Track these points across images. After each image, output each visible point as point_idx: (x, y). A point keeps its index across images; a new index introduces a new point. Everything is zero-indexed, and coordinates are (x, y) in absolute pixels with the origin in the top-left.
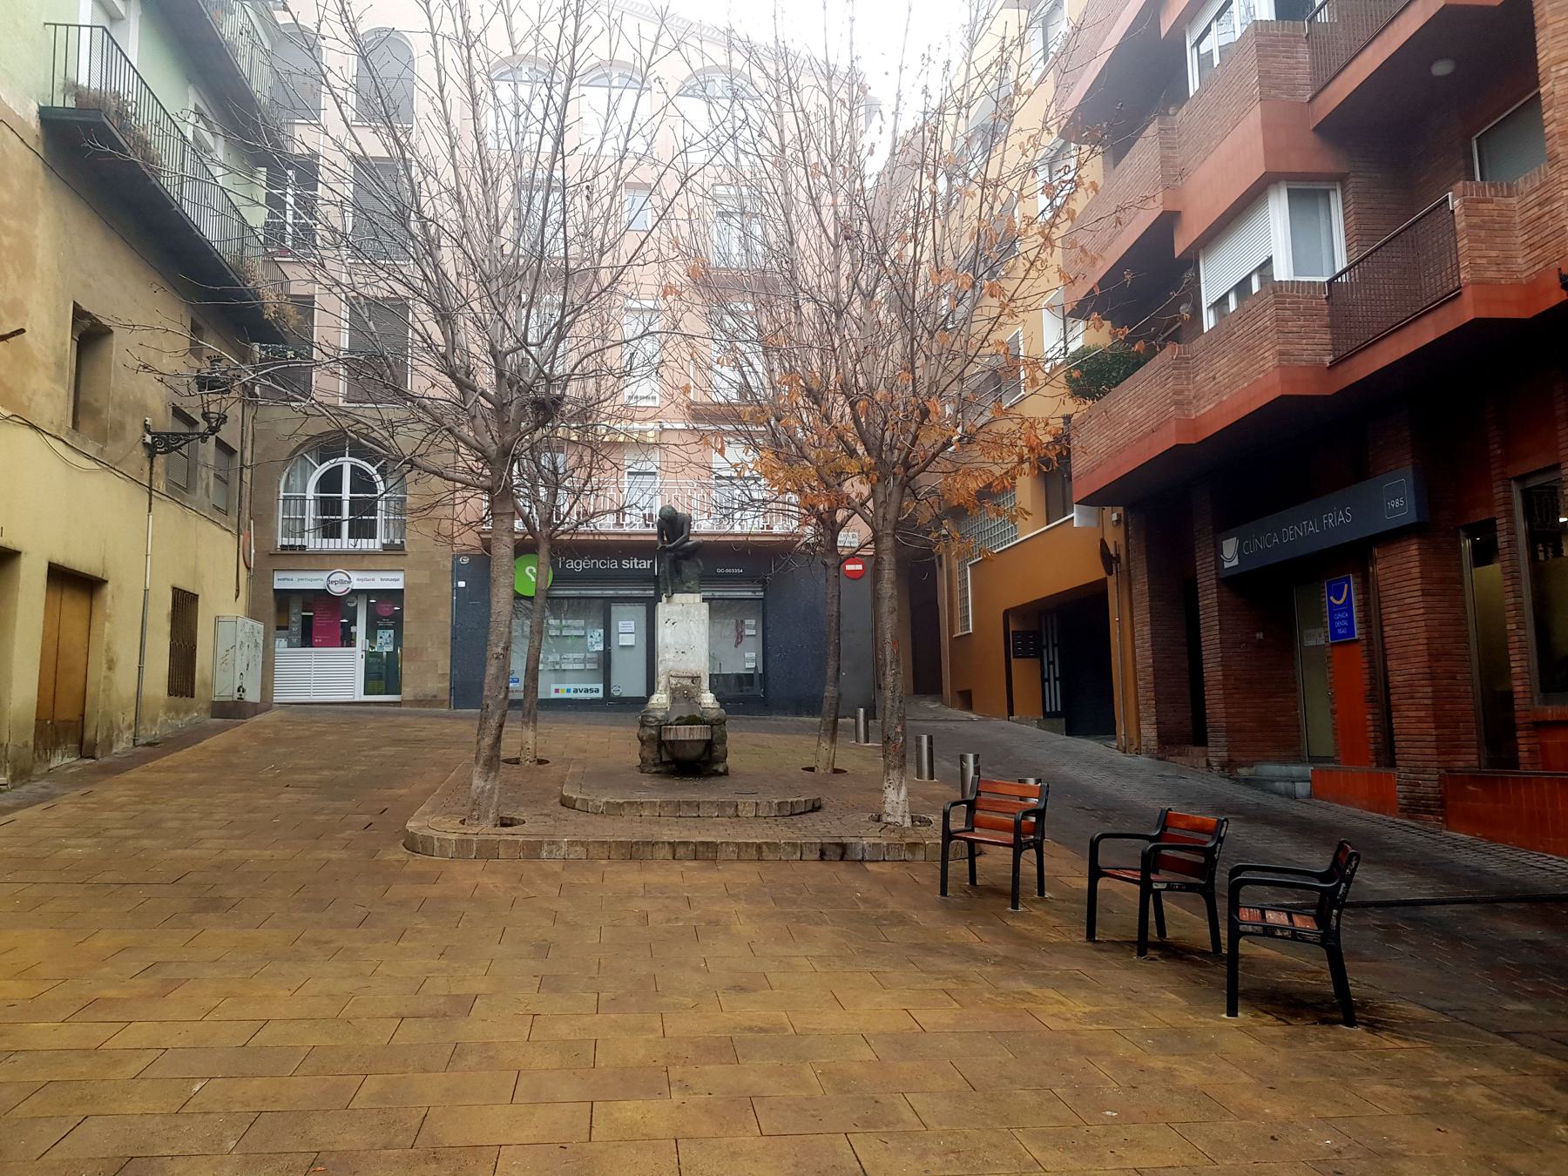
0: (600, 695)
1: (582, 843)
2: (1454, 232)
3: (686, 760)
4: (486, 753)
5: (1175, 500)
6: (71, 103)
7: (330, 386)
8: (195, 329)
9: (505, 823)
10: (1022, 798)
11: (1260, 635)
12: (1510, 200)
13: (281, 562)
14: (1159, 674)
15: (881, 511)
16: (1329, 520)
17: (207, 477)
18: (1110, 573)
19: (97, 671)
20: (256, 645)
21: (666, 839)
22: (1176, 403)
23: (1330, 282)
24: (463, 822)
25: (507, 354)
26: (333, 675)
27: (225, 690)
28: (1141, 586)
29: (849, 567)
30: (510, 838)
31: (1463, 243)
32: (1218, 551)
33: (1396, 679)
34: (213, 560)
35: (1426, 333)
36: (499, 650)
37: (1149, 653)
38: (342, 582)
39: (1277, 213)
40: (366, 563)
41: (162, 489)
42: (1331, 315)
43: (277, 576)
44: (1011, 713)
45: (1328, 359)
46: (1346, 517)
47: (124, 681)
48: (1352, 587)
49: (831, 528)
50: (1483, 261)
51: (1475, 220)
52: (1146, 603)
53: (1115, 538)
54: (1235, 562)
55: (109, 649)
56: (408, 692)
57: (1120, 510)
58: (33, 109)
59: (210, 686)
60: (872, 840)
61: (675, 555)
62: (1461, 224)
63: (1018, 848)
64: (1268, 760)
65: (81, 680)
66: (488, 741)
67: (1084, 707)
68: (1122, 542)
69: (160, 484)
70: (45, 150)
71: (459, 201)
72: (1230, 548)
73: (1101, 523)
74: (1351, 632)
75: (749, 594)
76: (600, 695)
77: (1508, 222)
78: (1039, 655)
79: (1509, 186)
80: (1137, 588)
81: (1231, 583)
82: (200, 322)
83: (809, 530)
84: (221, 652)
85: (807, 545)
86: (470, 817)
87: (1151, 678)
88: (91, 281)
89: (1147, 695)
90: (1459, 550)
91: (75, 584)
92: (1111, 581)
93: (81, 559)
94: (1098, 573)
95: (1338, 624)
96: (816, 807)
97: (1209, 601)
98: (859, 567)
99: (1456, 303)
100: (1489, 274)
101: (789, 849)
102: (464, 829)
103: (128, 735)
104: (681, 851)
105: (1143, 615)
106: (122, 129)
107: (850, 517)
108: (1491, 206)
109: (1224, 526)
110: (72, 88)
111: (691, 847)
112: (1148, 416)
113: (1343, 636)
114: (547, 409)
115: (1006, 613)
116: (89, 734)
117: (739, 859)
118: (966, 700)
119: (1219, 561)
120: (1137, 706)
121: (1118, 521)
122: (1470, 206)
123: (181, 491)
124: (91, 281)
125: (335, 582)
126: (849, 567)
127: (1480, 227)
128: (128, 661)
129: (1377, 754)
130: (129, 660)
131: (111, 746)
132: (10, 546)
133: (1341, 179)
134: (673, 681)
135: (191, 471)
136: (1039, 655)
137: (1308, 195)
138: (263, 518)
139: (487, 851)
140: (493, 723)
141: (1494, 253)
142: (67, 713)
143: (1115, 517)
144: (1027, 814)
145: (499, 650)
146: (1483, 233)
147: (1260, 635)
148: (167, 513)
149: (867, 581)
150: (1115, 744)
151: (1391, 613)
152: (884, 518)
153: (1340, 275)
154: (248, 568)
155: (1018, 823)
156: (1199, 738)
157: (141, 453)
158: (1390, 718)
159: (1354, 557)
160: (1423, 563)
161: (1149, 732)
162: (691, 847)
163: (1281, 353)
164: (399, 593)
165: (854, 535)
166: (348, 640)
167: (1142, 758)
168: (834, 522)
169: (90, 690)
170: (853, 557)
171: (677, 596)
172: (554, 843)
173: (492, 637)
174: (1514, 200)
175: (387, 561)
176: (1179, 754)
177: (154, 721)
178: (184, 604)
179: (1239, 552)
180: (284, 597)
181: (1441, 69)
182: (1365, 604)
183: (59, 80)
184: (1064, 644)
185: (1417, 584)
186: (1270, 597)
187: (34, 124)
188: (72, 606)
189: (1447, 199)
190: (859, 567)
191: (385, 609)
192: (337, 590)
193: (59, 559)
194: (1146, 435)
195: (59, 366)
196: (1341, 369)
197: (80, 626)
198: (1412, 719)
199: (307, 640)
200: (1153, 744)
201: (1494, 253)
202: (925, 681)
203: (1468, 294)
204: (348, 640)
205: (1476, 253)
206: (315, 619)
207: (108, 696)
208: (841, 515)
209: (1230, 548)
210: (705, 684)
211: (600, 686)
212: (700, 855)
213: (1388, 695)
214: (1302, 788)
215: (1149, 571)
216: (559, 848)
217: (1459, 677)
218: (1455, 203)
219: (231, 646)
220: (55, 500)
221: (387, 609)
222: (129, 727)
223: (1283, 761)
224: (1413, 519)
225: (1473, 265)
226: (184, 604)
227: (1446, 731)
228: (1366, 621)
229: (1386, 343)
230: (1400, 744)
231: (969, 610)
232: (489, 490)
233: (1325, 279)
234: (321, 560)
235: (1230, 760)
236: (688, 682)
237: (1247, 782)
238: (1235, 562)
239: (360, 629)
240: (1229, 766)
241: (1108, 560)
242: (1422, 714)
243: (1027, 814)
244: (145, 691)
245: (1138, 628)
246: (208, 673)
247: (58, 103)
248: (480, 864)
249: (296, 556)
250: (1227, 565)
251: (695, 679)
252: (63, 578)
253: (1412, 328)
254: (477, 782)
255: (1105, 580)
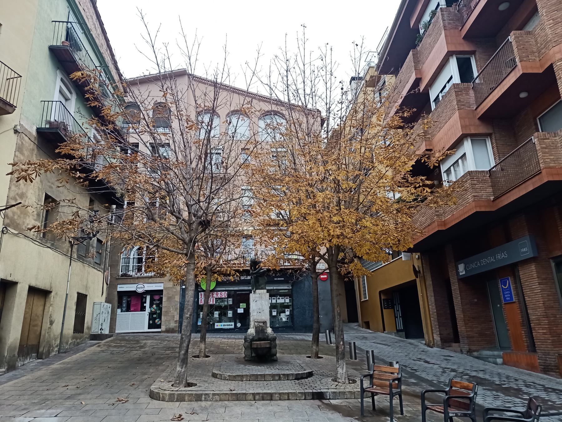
0: (233, 327)
1: (218, 394)
2: (536, 151)
3: (262, 353)
4: (182, 357)
5: (437, 250)
6: (48, 126)
7: (140, 221)
8: (91, 202)
9: (189, 385)
10: (392, 373)
11: (476, 300)
12: (555, 138)
13: (120, 281)
14: (439, 315)
15: (331, 258)
16: (499, 257)
17: (93, 251)
18: (417, 277)
19: (46, 325)
20: (108, 313)
21: (251, 392)
22: (437, 215)
23: (490, 171)
24: (172, 385)
25: (192, 205)
26: (136, 322)
27: (95, 330)
28: (429, 282)
29: (322, 277)
30: (190, 392)
31: (540, 154)
32: (457, 269)
33: (532, 317)
34: (94, 282)
35: (530, 187)
36: (188, 316)
37: (434, 307)
38: (140, 288)
39: (467, 146)
40: (150, 280)
41: (76, 257)
42: (492, 182)
43: (119, 286)
44: (384, 330)
45: (492, 198)
46: (505, 255)
47: (56, 329)
48: (510, 282)
49: (315, 264)
50: (548, 160)
51: (544, 146)
52: (431, 289)
53: (417, 264)
54: (464, 273)
55: (51, 317)
56: (163, 328)
57: (419, 254)
58: (35, 128)
59: (89, 328)
60: (333, 390)
61: (258, 275)
62: (538, 148)
63: (392, 395)
64: (484, 349)
65: (39, 329)
66: (183, 352)
67: (411, 328)
68: (421, 266)
69: (75, 255)
70: (38, 142)
71: (176, 153)
72: (461, 267)
73: (412, 259)
74: (511, 297)
75: (286, 288)
76: (233, 327)
77: (556, 146)
78: (393, 308)
79: (555, 134)
80: (427, 283)
81: (463, 280)
82: (93, 198)
83: (307, 265)
84: (95, 316)
85: (306, 269)
86: (176, 383)
87: (436, 317)
88: (52, 186)
89: (435, 324)
90: (550, 267)
91: (39, 293)
92: (418, 280)
93: (41, 284)
94: (414, 277)
95: (506, 296)
96: (310, 375)
97: (455, 287)
98: (326, 276)
99: (540, 176)
100: (551, 165)
101: (300, 395)
102: (173, 388)
103: (56, 349)
104: (257, 397)
105: (431, 293)
106: (66, 135)
107: (320, 260)
108: (548, 141)
109: (459, 259)
110: (50, 123)
111: (261, 395)
112: (426, 220)
113: (509, 300)
114: (205, 224)
115: (380, 292)
116: (41, 350)
117: (280, 400)
118: (367, 325)
119: (458, 273)
120: (432, 327)
121: (418, 258)
122: (541, 140)
123: (82, 258)
124: (52, 186)
125: (139, 288)
126: (322, 277)
127: (546, 148)
128: (59, 319)
129: (528, 347)
130: (59, 319)
131: (49, 354)
132: (14, 281)
133: (489, 135)
134: (256, 324)
135: (87, 251)
136: (393, 308)
137: (477, 138)
138: (114, 265)
139: (181, 398)
140: (185, 345)
141: (552, 157)
142: (33, 341)
143: (417, 257)
144: (394, 380)
145: (188, 316)
146: (547, 150)
147: (476, 300)
148: (77, 265)
149: (329, 281)
150: (424, 342)
151: (527, 292)
152: (332, 260)
153: (493, 168)
154: (107, 284)
155: (391, 385)
156: (456, 339)
157: (67, 244)
158: (532, 333)
159: (512, 269)
160: (538, 272)
161: (437, 338)
162: (261, 395)
163: (474, 196)
164: (162, 291)
165: (322, 266)
166: (143, 309)
167: (435, 349)
168: (314, 261)
169: (43, 332)
170: (322, 274)
171: (257, 291)
172: (206, 394)
173: (185, 311)
174: (557, 138)
175: (158, 280)
176: (449, 347)
177: (67, 343)
178: (82, 299)
179: (465, 269)
180: (121, 294)
181: (523, 95)
182: (516, 288)
183: (44, 119)
184: (402, 302)
185: (536, 281)
186: (481, 286)
187: (34, 133)
188: (38, 302)
189: (532, 139)
190: (326, 276)
191: (156, 297)
192: (140, 291)
193: (33, 284)
194: (426, 227)
195: (38, 215)
196: (497, 201)
197: (41, 308)
198: (539, 333)
199: (128, 310)
200: (439, 343)
201: (552, 157)
202: (352, 318)
203: (544, 172)
204: (143, 309)
205: (545, 157)
206: (129, 301)
207: (49, 335)
208: (317, 259)
209: (461, 267)
210: (268, 325)
211: (233, 323)
212: (265, 398)
213: (530, 324)
214: (499, 361)
215: (432, 277)
216: (209, 397)
217: (558, 316)
218: (535, 140)
219: (98, 314)
220: (29, 262)
221: (156, 295)
222: (57, 346)
223: (490, 349)
224: (532, 256)
225: (545, 162)
226: (82, 299)
227: (555, 338)
228: (517, 295)
229: (514, 191)
230: (537, 344)
231: (365, 293)
232: (186, 255)
233: (488, 170)
234: (135, 280)
235: (469, 349)
236: (261, 324)
237: (477, 358)
238: (464, 273)
239: (147, 305)
240: (470, 352)
241: (416, 272)
242: (545, 331)
243: (394, 380)
244: (64, 331)
245: (429, 298)
246: (90, 324)
247: (43, 126)
248: (178, 403)
249: (126, 277)
250: (461, 274)
251: (265, 323)
252: (33, 291)
253: (523, 186)
254: (178, 369)
255: (415, 280)
